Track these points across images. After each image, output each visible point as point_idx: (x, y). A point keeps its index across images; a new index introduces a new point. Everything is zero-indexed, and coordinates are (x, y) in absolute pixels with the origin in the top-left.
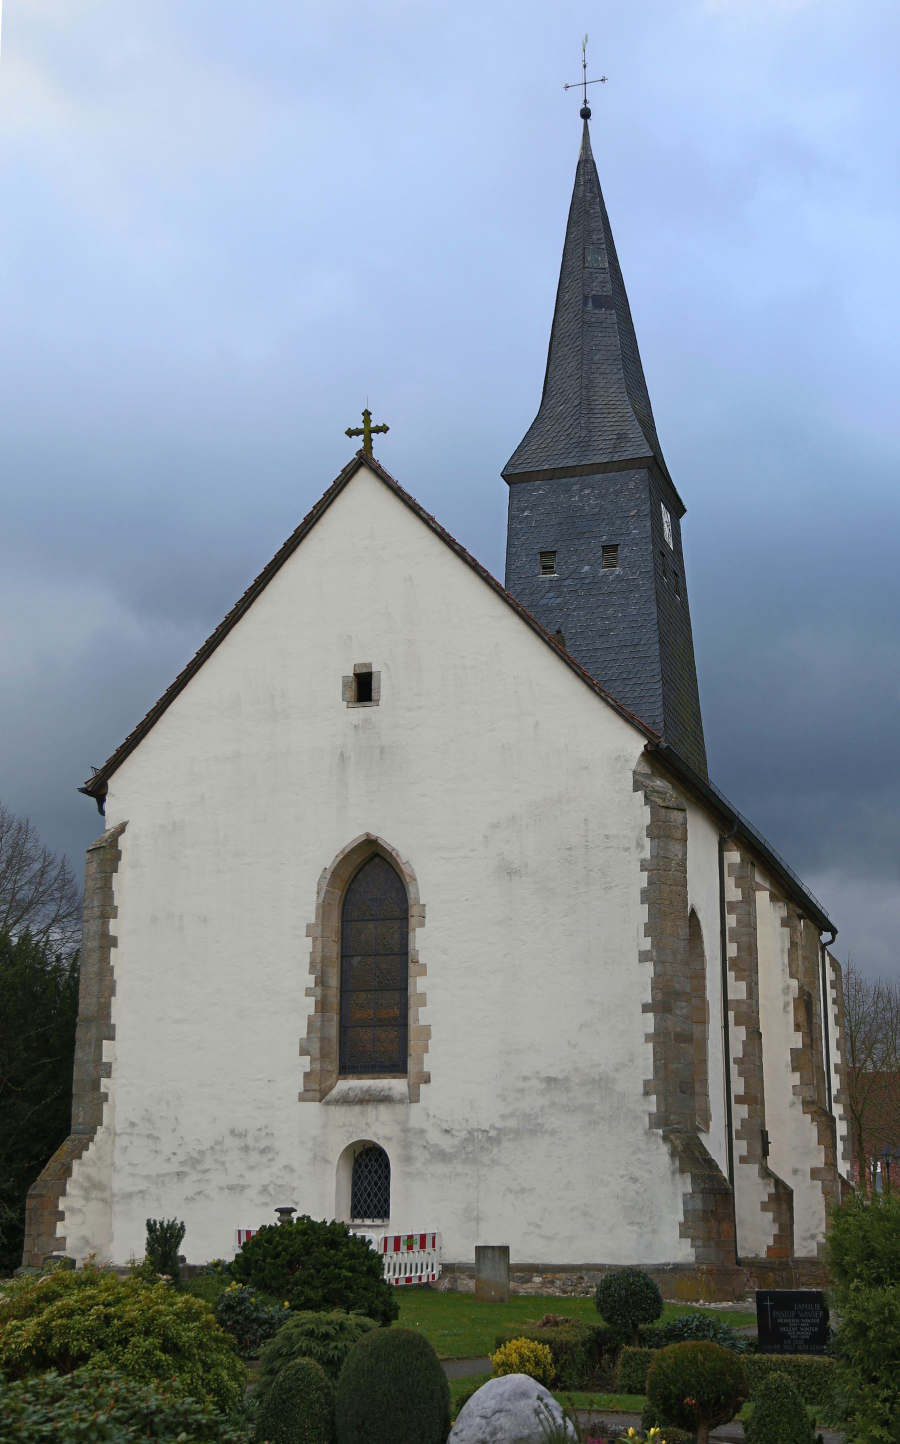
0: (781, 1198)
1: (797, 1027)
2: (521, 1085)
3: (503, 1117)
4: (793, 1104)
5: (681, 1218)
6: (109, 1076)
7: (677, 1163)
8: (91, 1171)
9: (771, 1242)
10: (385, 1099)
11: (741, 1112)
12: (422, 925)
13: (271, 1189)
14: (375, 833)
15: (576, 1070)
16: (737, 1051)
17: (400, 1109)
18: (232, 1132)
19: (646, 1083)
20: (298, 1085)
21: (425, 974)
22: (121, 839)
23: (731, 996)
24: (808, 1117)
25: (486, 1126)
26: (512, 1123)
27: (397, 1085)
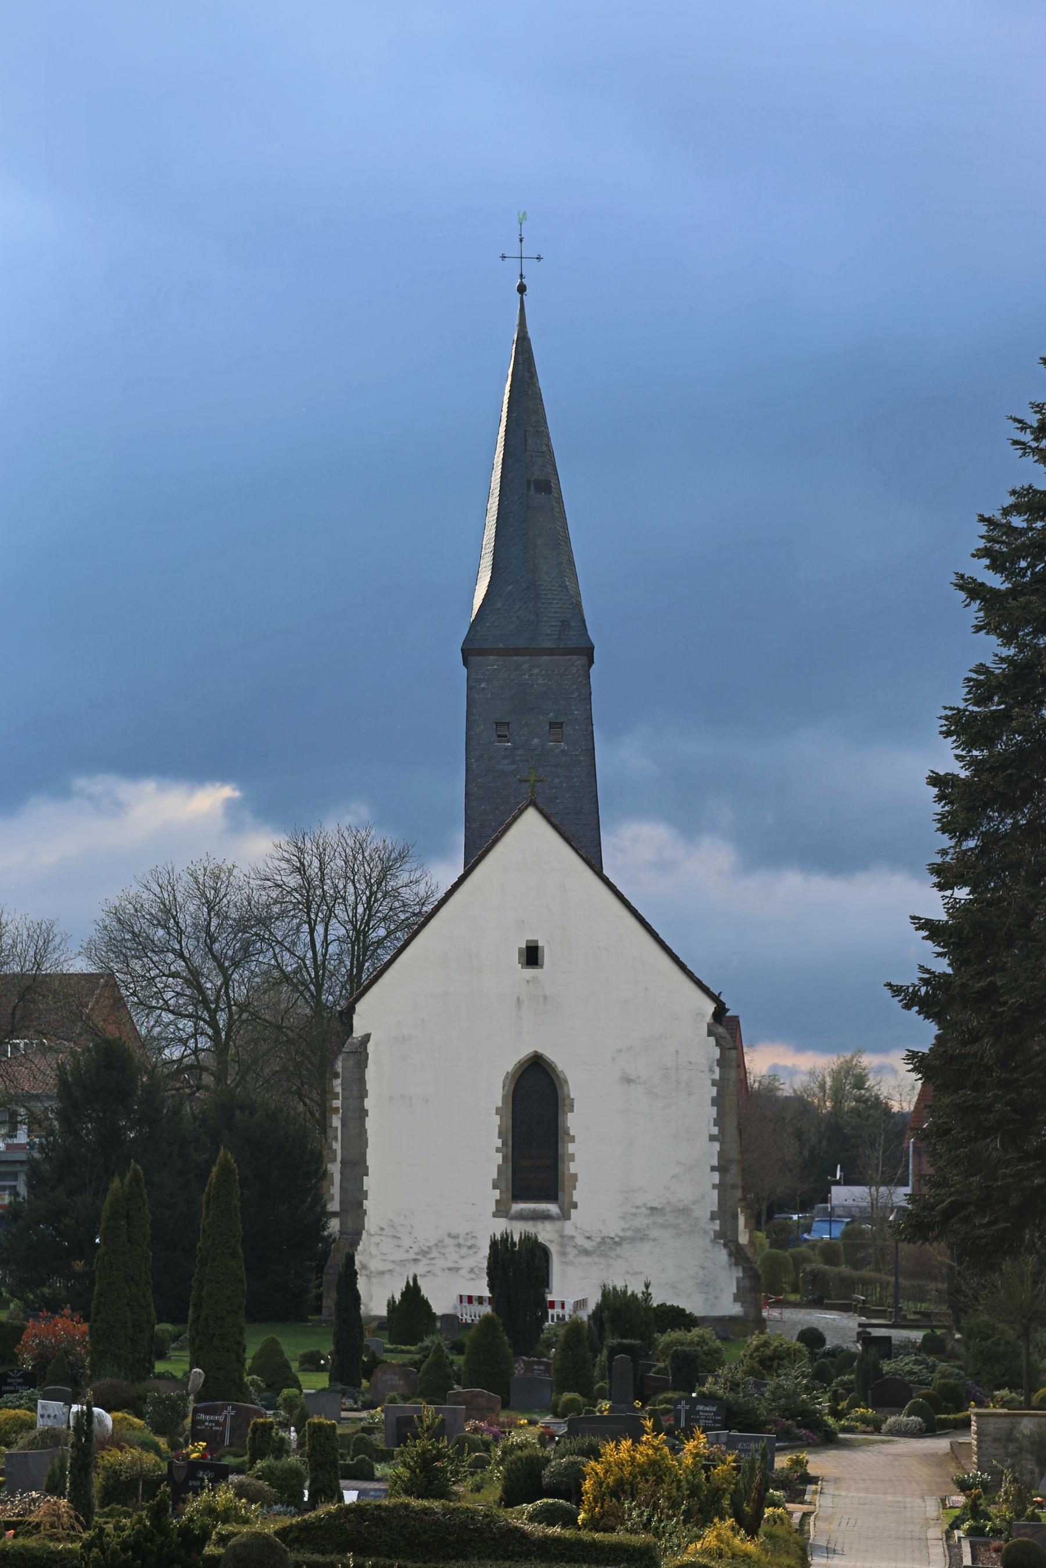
2: (635, 1211)
3: (623, 1230)
5: (735, 1290)
7: (733, 1260)
12: (572, 1111)
13: (476, 1270)
14: (540, 1051)
15: (669, 1203)
17: (558, 1224)
18: (449, 1235)
19: (712, 1213)
21: (574, 1141)
25: (612, 1235)
26: (629, 1234)
27: (553, 1208)
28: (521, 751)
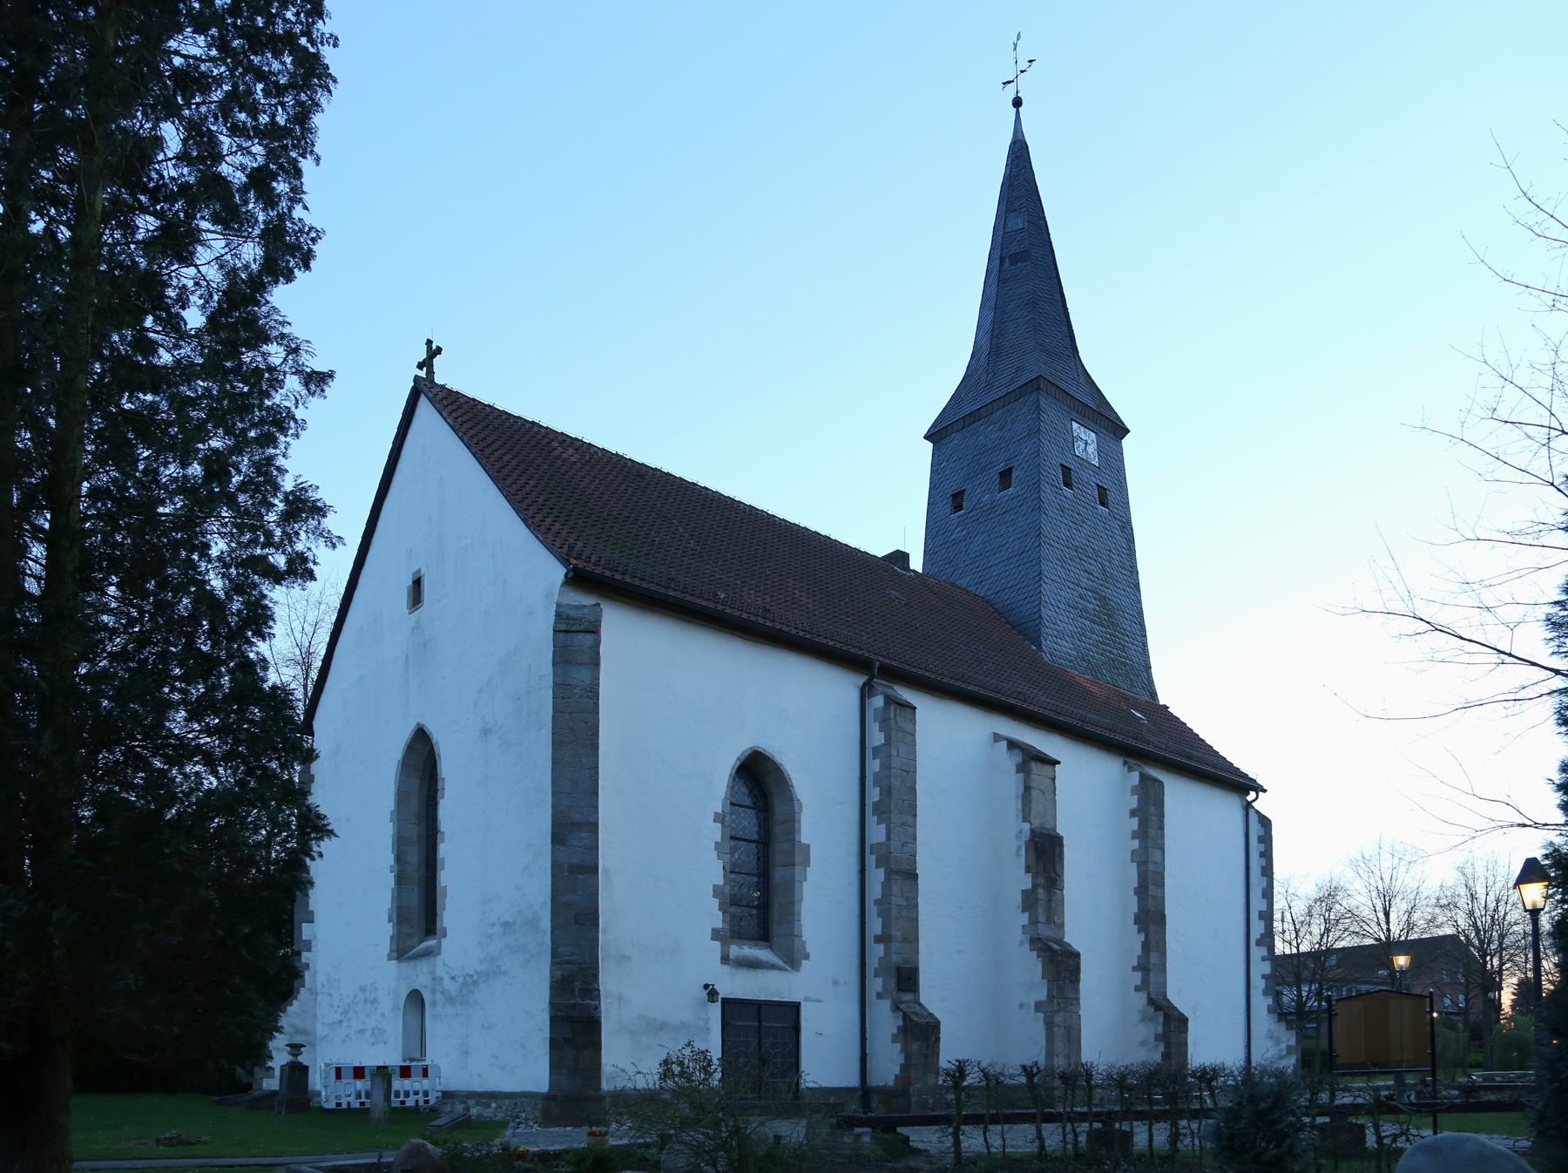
4: (1022, 943)
8: (296, 1021)
9: (897, 1070)
24: (1035, 954)
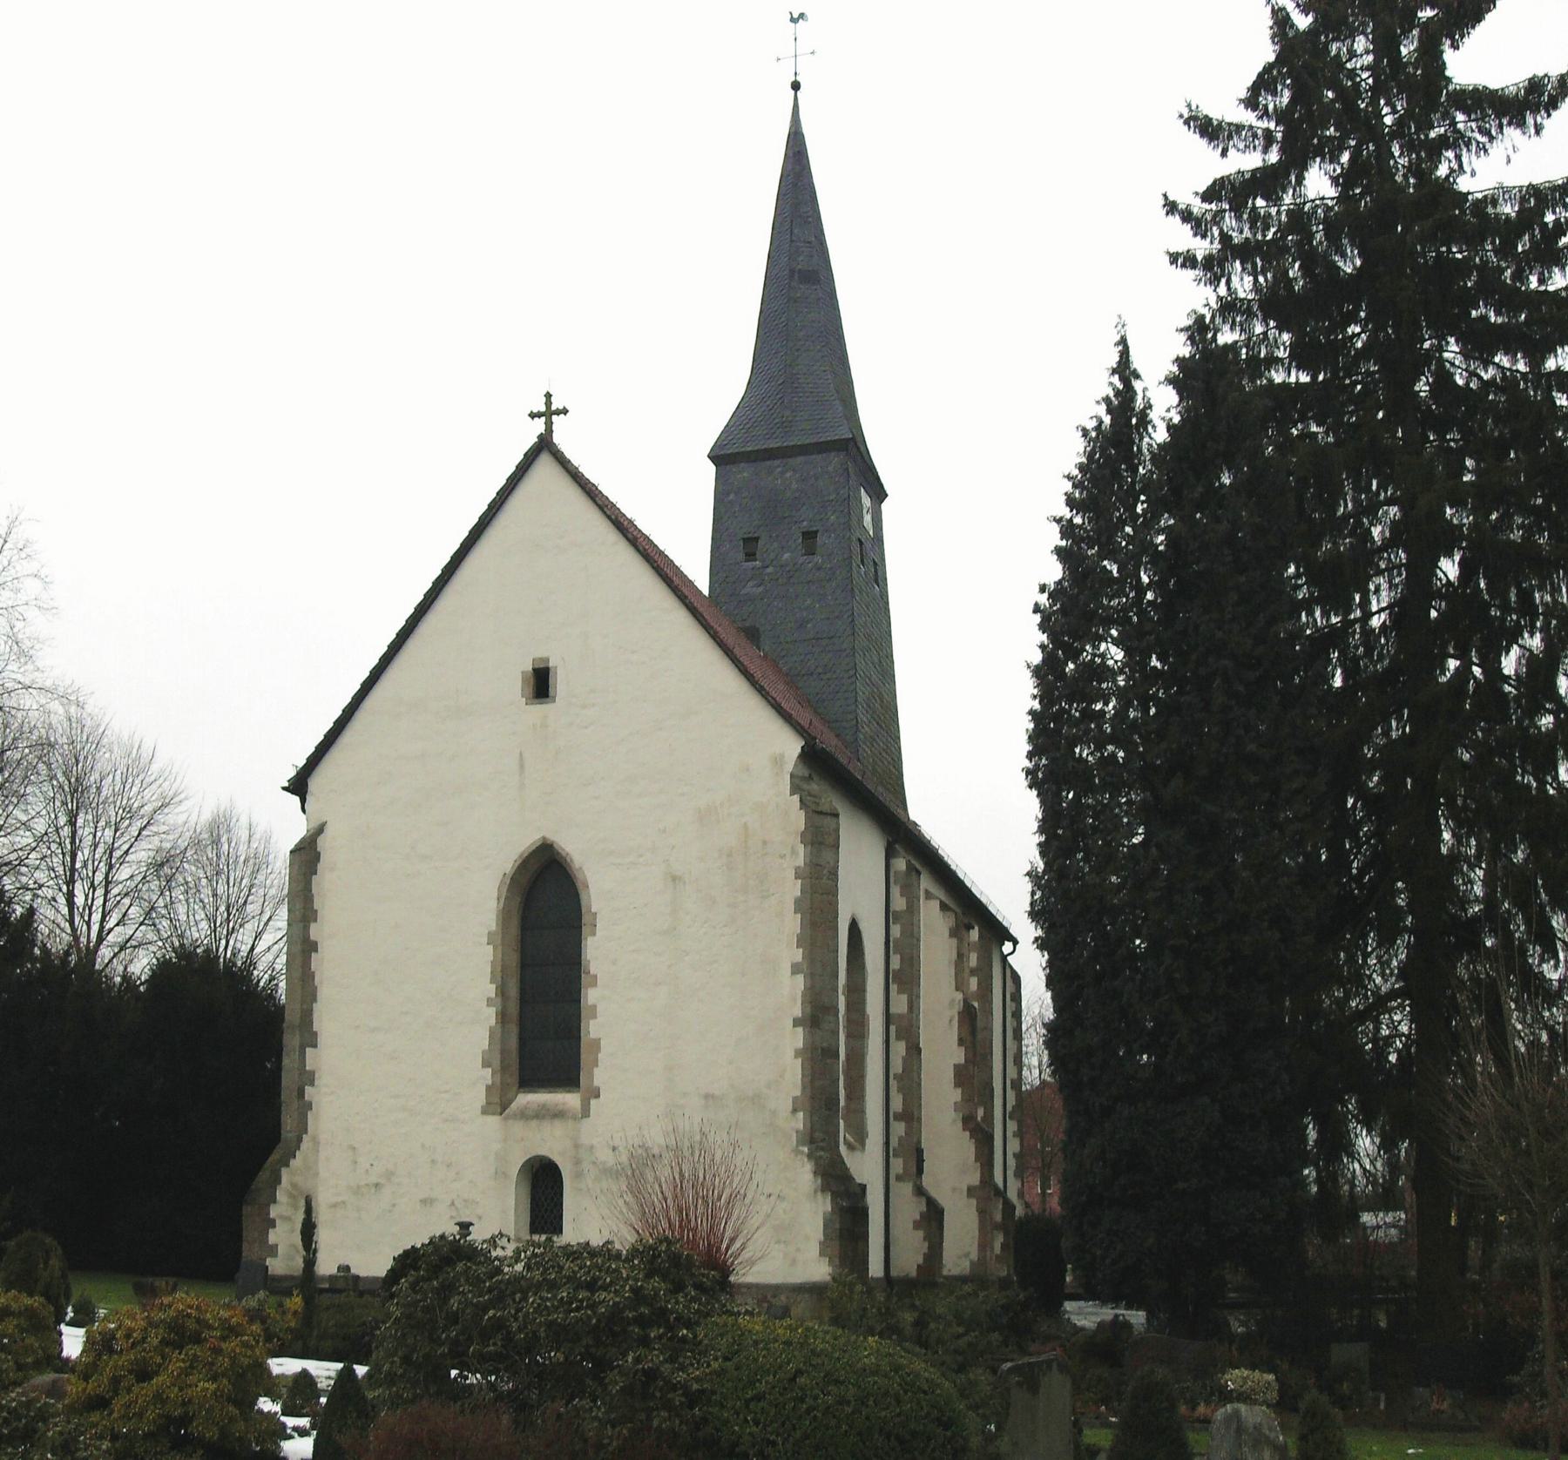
0: (933, 1217)
1: (961, 1042)
6: (312, 1084)
10: (558, 1114)
11: (899, 1128)
16: (897, 1066)
19: (795, 1099)
20: (481, 1098)
22: (320, 841)
23: (893, 1010)
27: (571, 1100)
28: (770, 570)
